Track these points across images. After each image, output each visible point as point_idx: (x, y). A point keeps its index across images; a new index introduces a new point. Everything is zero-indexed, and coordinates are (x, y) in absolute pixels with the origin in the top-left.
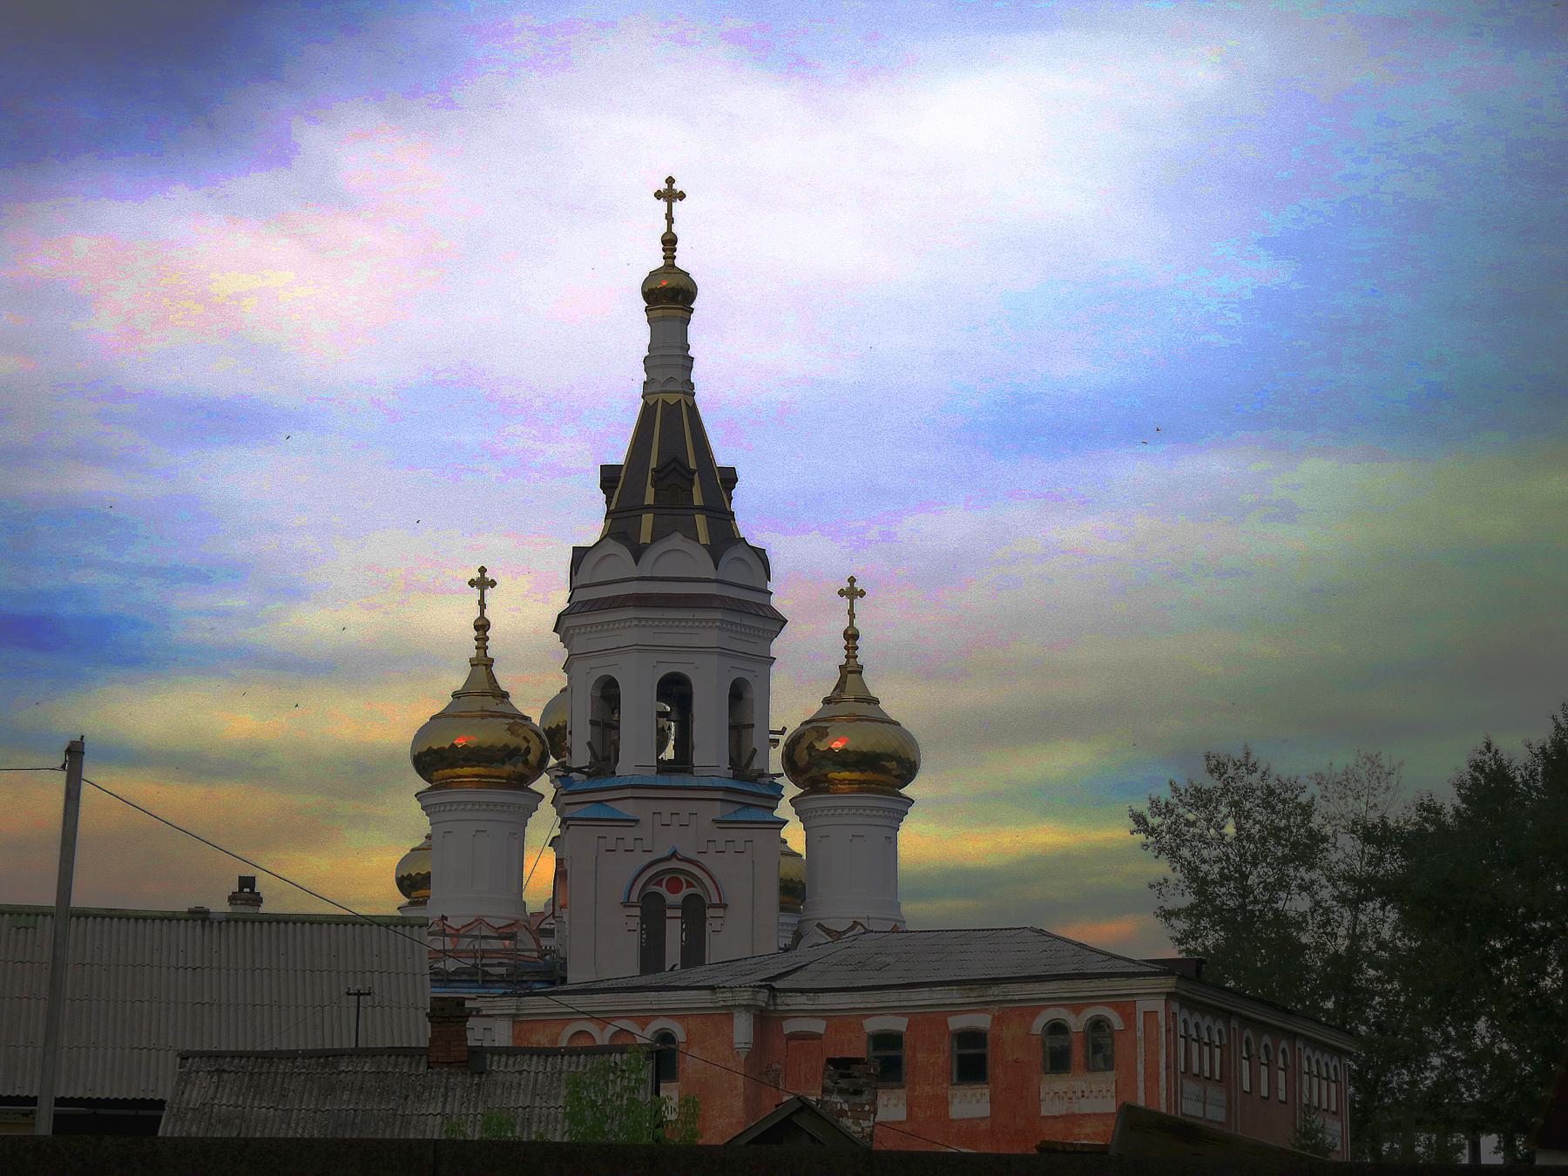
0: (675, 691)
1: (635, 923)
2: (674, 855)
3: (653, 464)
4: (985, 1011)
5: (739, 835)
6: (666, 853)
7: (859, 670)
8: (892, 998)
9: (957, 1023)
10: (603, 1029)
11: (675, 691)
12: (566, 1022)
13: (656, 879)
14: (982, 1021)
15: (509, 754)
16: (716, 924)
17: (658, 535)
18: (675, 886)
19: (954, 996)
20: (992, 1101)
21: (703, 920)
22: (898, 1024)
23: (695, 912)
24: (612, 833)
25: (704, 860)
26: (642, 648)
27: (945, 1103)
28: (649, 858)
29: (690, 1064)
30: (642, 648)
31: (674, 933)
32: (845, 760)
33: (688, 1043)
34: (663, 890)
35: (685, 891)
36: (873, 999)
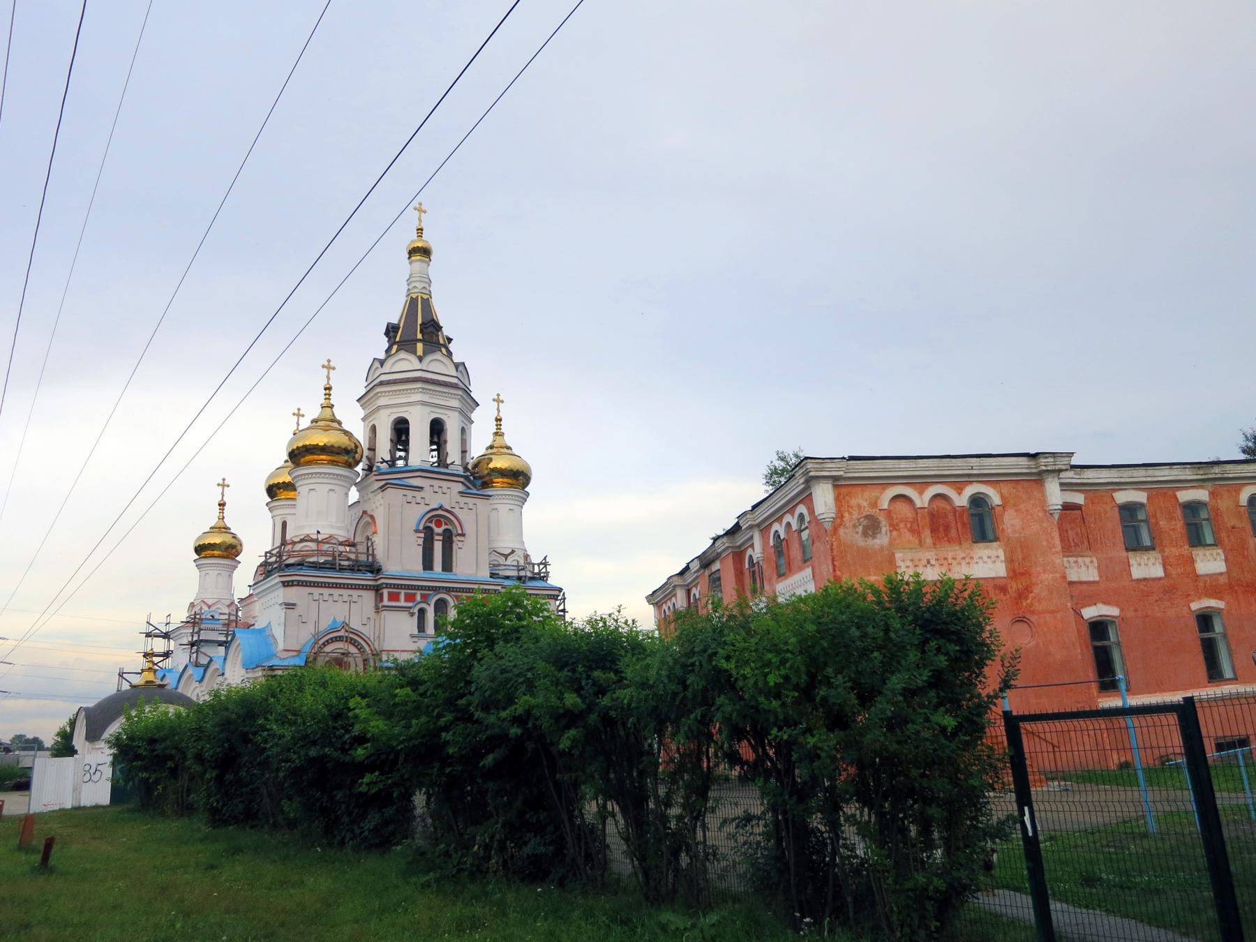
0: (437, 429)
1: (421, 541)
2: (441, 508)
3: (420, 321)
4: (1202, 487)
5: (470, 501)
6: (436, 506)
7: (502, 435)
8: (1140, 475)
9: (1185, 496)
10: (921, 493)
11: (437, 429)
12: (885, 486)
13: (430, 520)
14: (1202, 495)
15: (346, 451)
16: (460, 544)
17: (426, 353)
18: (439, 524)
19: (1188, 474)
20: (1226, 560)
21: (451, 542)
22: (1140, 497)
23: (448, 539)
24: (410, 493)
25: (455, 511)
26: (424, 403)
27: (1192, 561)
28: (429, 508)
29: (1010, 522)
30: (424, 403)
31: (438, 547)
32: (503, 473)
33: (1004, 506)
34: (433, 525)
35: (444, 527)
36: (1126, 476)
